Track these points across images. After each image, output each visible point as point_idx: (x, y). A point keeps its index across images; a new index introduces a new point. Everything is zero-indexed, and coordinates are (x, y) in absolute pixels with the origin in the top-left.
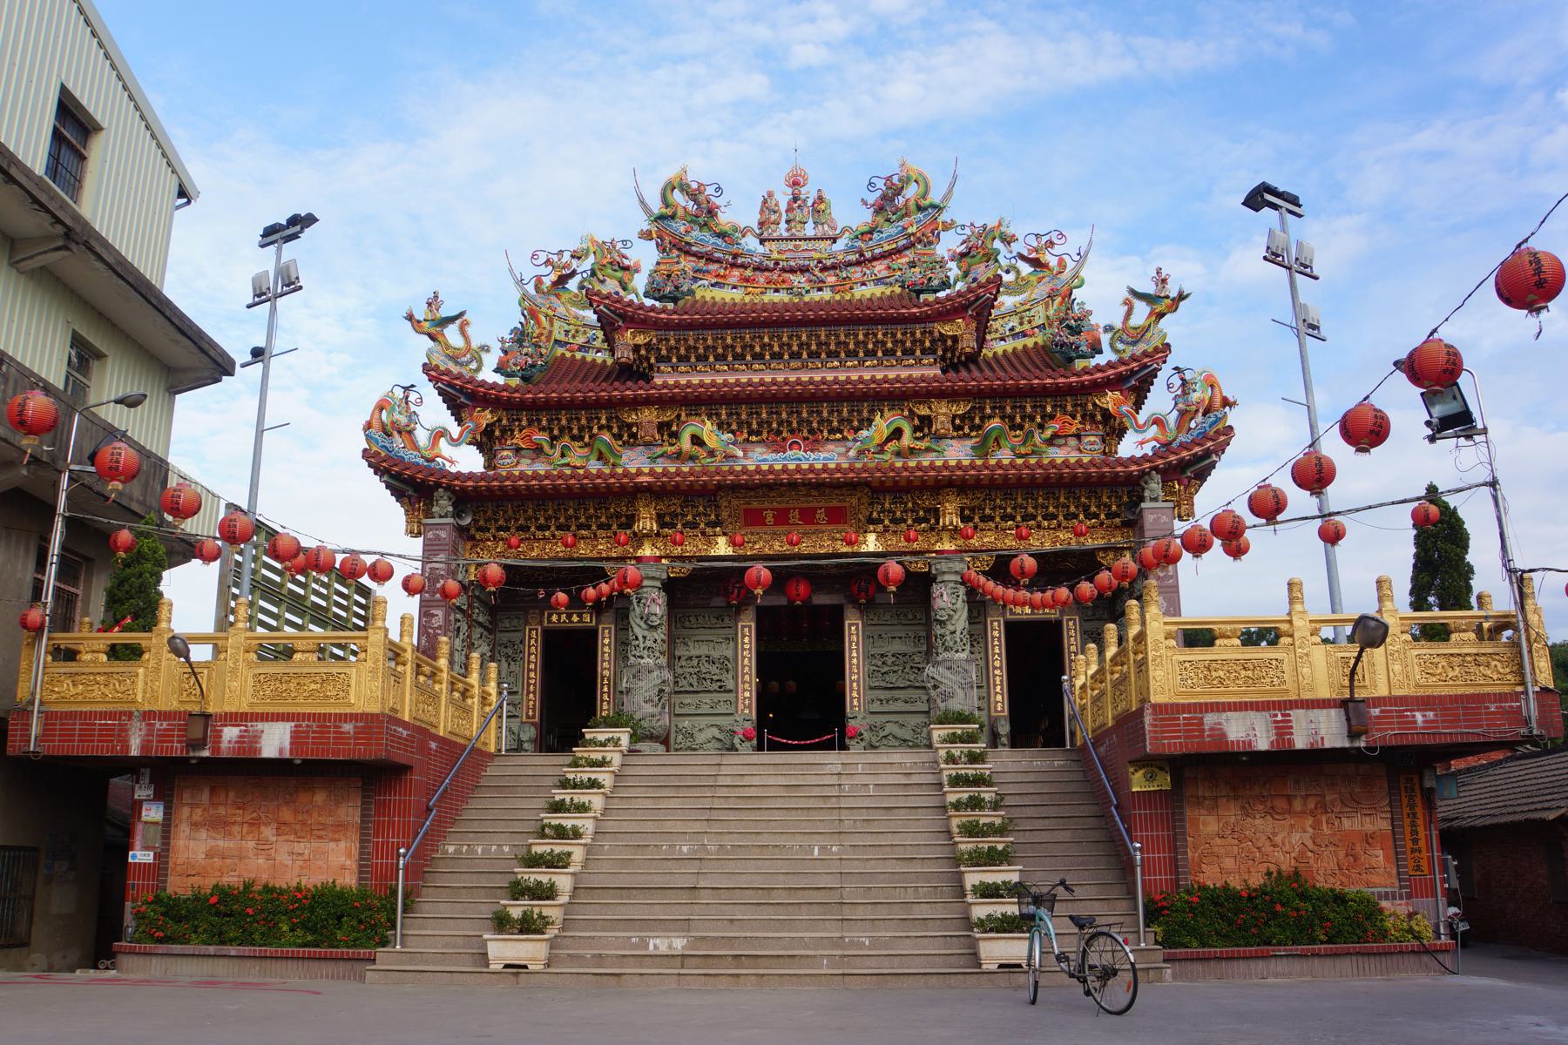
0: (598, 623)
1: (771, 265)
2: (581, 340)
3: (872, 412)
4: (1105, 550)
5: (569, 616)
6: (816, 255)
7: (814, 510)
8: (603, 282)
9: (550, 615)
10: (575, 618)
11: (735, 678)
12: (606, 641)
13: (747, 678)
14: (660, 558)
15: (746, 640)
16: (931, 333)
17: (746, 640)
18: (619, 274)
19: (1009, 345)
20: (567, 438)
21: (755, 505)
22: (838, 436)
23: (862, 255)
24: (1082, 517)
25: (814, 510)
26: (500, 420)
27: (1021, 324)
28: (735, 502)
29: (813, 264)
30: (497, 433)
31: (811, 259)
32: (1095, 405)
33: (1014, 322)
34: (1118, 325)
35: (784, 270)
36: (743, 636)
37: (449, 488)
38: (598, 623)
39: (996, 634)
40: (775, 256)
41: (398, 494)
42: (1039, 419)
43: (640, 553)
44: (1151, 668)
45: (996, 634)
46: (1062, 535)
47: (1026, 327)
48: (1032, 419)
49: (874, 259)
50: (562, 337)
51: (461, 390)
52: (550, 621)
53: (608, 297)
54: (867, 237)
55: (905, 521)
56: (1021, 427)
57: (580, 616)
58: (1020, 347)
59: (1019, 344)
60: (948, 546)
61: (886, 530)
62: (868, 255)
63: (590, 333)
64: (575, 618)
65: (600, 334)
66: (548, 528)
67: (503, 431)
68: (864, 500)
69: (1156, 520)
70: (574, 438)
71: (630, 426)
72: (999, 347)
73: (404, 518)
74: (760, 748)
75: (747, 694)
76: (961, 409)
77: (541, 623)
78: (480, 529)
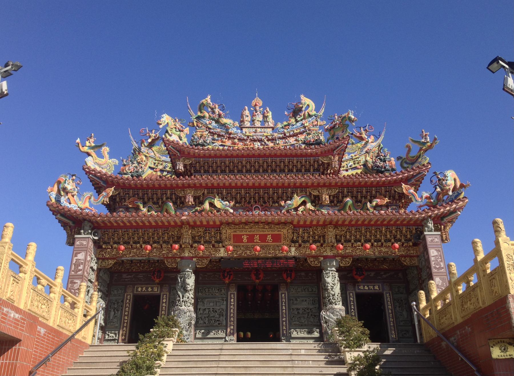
0: (161, 291)
1: (246, 138)
2: (160, 167)
3: (293, 193)
4: (405, 257)
5: (147, 289)
6: (265, 134)
7: (266, 235)
8: (171, 136)
9: (137, 288)
10: (150, 289)
11: (226, 319)
12: (164, 301)
13: (232, 319)
14: (193, 257)
15: (232, 300)
16: (317, 162)
17: (232, 300)
18: (178, 133)
19: (350, 172)
20: (151, 203)
21: (238, 233)
22: (277, 204)
23: (285, 135)
24: (393, 240)
25: (266, 235)
26: (119, 194)
27: (354, 164)
28: (229, 231)
29: (263, 138)
30: (118, 200)
31: (263, 136)
32: (395, 191)
33: (351, 163)
34: (404, 156)
35: (251, 140)
36: (231, 298)
37: (90, 221)
38: (161, 291)
39: (352, 299)
40: (248, 134)
41: (64, 225)
42: (369, 197)
43: (183, 255)
44: (508, 272)
45: (352, 299)
46: (383, 249)
47: (356, 165)
48: (366, 197)
49: (290, 136)
50: (152, 166)
51: (100, 178)
52: (137, 291)
53: (173, 142)
54: (287, 127)
55: (309, 242)
56: (360, 202)
57: (152, 288)
58: (354, 173)
59: (354, 172)
60: (329, 253)
61: (300, 245)
62: (288, 134)
63: (164, 164)
64: (150, 289)
65: (170, 165)
66: (139, 243)
67: (121, 199)
68: (289, 231)
69: (432, 241)
70: (154, 203)
71: (180, 198)
72: (345, 173)
73: (66, 236)
74: (239, 340)
75: (232, 327)
76: (334, 192)
77: (133, 292)
78: (105, 243)
